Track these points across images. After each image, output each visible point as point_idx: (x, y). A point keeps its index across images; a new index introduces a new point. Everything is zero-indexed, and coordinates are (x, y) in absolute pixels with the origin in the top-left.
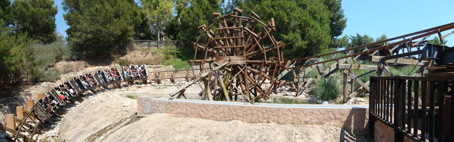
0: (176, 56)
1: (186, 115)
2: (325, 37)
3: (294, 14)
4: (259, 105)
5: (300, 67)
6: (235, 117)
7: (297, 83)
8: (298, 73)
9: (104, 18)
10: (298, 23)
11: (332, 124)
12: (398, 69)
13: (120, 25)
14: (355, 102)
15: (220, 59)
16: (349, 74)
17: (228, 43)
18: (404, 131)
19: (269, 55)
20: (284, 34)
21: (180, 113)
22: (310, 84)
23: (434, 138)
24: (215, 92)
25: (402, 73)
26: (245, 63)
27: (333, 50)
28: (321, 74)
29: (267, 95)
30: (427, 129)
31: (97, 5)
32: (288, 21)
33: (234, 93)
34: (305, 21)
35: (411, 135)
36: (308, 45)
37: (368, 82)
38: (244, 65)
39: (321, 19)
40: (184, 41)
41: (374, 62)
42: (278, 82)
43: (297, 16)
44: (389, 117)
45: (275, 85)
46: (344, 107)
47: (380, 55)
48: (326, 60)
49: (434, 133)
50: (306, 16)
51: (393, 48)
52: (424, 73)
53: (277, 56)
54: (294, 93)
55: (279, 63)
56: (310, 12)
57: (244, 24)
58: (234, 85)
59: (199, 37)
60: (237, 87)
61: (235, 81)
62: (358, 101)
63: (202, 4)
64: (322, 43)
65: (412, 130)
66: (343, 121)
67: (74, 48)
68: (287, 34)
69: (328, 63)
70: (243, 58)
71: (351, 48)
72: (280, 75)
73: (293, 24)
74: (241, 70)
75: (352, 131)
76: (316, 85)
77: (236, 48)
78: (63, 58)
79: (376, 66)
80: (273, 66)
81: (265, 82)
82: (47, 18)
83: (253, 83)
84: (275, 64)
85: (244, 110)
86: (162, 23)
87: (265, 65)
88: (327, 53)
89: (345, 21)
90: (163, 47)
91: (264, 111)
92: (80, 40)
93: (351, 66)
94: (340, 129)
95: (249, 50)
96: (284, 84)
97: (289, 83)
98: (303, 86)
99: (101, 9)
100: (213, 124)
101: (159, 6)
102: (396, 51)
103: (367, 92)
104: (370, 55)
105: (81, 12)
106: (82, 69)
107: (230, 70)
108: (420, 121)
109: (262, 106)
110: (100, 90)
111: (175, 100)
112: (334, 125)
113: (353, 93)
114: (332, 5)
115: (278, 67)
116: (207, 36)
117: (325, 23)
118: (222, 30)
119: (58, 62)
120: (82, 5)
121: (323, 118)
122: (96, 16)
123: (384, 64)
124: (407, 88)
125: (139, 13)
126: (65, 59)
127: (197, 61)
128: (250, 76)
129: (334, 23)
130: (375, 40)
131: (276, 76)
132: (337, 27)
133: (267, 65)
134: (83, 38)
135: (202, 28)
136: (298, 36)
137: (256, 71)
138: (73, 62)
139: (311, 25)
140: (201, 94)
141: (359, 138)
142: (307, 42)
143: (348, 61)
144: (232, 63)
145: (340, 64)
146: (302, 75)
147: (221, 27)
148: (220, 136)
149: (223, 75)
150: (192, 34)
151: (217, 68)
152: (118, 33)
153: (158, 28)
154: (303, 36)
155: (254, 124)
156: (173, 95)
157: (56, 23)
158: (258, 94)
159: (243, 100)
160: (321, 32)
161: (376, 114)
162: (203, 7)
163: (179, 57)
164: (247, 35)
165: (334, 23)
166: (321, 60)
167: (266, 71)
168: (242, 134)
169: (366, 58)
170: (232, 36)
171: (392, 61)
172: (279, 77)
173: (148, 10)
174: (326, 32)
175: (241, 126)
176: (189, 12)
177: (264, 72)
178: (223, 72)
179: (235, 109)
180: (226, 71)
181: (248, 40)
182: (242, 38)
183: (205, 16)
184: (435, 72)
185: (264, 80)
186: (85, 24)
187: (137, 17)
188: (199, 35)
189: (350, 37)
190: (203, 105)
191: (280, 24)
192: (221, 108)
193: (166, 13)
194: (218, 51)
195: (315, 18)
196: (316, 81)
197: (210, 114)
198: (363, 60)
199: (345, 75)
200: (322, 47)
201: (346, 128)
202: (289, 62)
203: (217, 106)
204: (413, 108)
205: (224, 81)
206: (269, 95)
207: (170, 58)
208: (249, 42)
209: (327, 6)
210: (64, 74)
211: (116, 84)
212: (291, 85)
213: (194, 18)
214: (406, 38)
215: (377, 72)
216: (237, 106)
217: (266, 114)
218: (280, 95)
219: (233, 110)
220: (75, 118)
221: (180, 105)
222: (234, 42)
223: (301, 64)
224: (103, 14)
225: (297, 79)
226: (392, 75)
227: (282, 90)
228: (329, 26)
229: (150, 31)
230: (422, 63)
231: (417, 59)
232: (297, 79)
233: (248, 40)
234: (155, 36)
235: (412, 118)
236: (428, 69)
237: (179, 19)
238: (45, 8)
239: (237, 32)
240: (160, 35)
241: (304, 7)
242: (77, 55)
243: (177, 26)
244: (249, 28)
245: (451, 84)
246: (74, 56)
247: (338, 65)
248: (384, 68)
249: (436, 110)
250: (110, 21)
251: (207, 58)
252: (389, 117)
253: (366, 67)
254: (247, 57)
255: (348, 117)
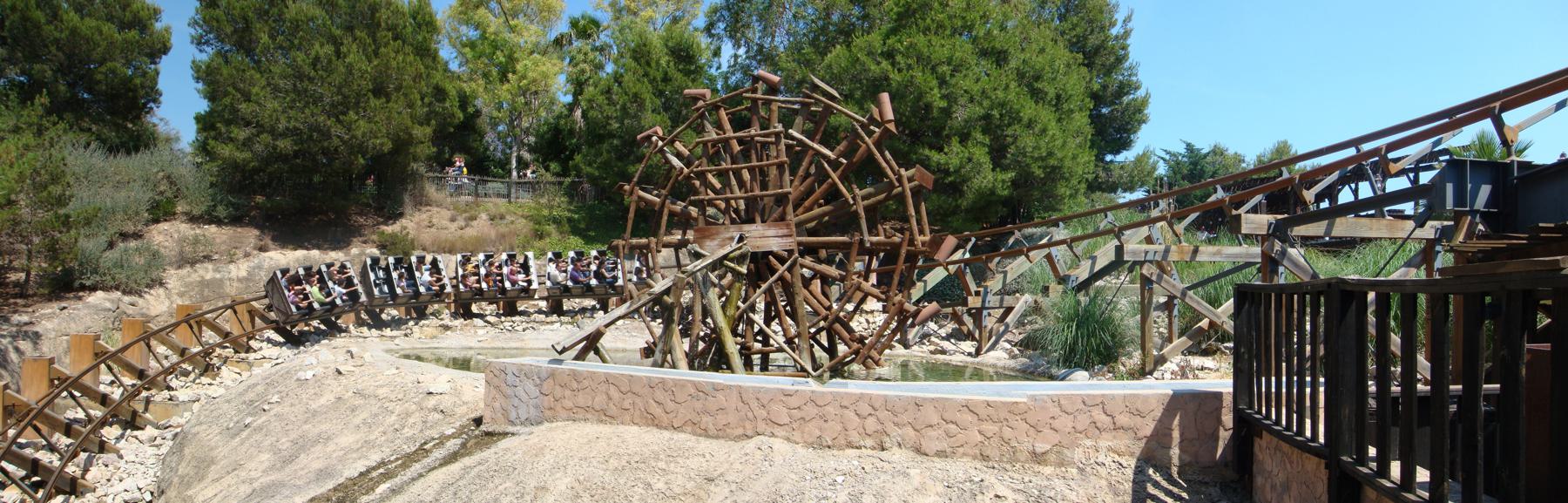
0: (567, 227)
1: (605, 416)
2: (1074, 157)
3: (964, 83)
4: (846, 385)
5: (990, 259)
6: (761, 427)
7: (980, 310)
8: (980, 277)
9: (339, 92)
10: (979, 111)
11: (1104, 443)
12: (1336, 254)
13: (388, 118)
14: (1183, 372)
15: (710, 236)
16: (1160, 278)
17: (734, 182)
18: (1365, 470)
19: (876, 215)
20: (931, 147)
21: (586, 409)
22: (1024, 315)
23: (1484, 497)
24: (693, 346)
25: (1351, 268)
26: (795, 247)
27: (1101, 199)
28: (1062, 280)
29: (874, 353)
30: (1453, 463)
31: (317, 46)
32: (943, 104)
33: (758, 346)
34: (1002, 105)
35: (1389, 485)
36: (1015, 183)
37: (1228, 305)
38: (791, 252)
39: (1058, 97)
40: (593, 180)
41: (1246, 236)
42: (913, 308)
43: (976, 88)
44: (1308, 422)
45: (903, 320)
46: (1145, 387)
47: (1271, 209)
48: (1079, 233)
49: (1480, 479)
50: (1007, 86)
51: (1317, 183)
52: (1438, 264)
53: (906, 219)
54: (968, 346)
55: (911, 242)
56: (1021, 75)
57: (787, 119)
58: (759, 318)
59: (641, 167)
60: (768, 325)
61: (761, 306)
62: (1192, 370)
63: (648, 64)
64: (1063, 177)
65: (1395, 468)
66: (1141, 434)
67: (223, 182)
68: (940, 150)
69: (1086, 242)
70: (785, 231)
71: (1165, 190)
72: (920, 285)
73: (960, 115)
74: (782, 269)
75: (1174, 471)
76: (1044, 317)
77: (762, 197)
78: (179, 209)
79: (1257, 250)
80: (891, 254)
81: (866, 307)
82: (128, 63)
83: (824, 312)
84: (898, 246)
85: (794, 402)
86: (525, 124)
87: (863, 250)
88: (1081, 210)
89: (1145, 102)
90: (526, 200)
91: (865, 409)
92: (247, 155)
93: (1167, 251)
94: (1133, 463)
95: (807, 203)
96: (934, 317)
97: (950, 310)
98: (1002, 319)
99: (330, 61)
100: (692, 449)
101: (514, 72)
102: (1331, 193)
103: (1224, 338)
104: (1234, 212)
105: (258, 62)
106: (247, 255)
107: (744, 270)
108: (1423, 437)
109: (858, 391)
110: (309, 333)
111: (569, 364)
112: (1110, 449)
113: (1176, 342)
114: (1097, 50)
115: (912, 258)
116: (667, 161)
117: (1072, 111)
118: (715, 143)
119: (157, 221)
120: (265, 38)
121: (1070, 425)
122: (311, 80)
123: (1283, 241)
124: (1371, 319)
125: (453, 93)
126: (186, 214)
127: (634, 241)
128: (812, 287)
129: (1104, 111)
130: (1250, 161)
131: (906, 285)
132: (1114, 121)
133: (871, 252)
134: (258, 148)
135: (649, 137)
136: (981, 155)
137: (833, 271)
138: (213, 228)
139: (1025, 120)
140: (648, 352)
141: (1198, 493)
142: (1011, 175)
143: (1156, 233)
144: (748, 247)
145: (1128, 247)
146: (995, 284)
147: (712, 134)
148: (720, 491)
149: (721, 287)
150: (620, 158)
151: (700, 264)
152: (382, 145)
153: (513, 137)
154: (998, 155)
155: (829, 452)
156: (564, 350)
157: (162, 84)
158: (842, 349)
159: (790, 371)
160: (1059, 142)
161: (1260, 412)
162: (652, 72)
163: (576, 231)
164: (797, 154)
165: (1104, 111)
166: (1061, 233)
167: (868, 270)
168: (787, 487)
169: (1218, 222)
170: (747, 158)
171: (1315, 229)
172: (917, 292)
173: (481, 82)
174: (1078, 140)
175: (784, 456)
176: (608, 91)
177: (859, 274)
178: (721, 277)
179: (763, 399)
180: (729, 275)
181: (801, 172)
182: (780, 166)
183: (658, 102)
184: (1480, 260)
185: (863, 301)
186: (272, 104)
187: (447, 104)
188: (640, 159)
189: (1163, 155)
190: (663, 382)
191: (914, 113)
192: (720, 396)
193: (536, 93)
194: (703, 211)
195: (1037, 95)
196: (1045, 302)
197: (684, 413)
198: (1210, 229)
199: (1146, 282)
200: (1062, 190)
201: (1152, 457)
202: (951, 241)
203: (708, 389)
204: (1395, 389)
205: (724, 307)
206: (880, 353)
207: (549, 235)
208: (805, 178)
209: (1080, 56)
210: (179, 267)
211: (367, 312)
212: (956, 318)
213: (624, 108)
214: (1366, 147)
215: (1259, 270)
216: (768, 390)
217: (871, 420)
218: (920, 352)
219: (754, 404)
220: (231, 433)
221: (586, 383)
222: (753, 179)
223: (991, 248)
224: (337, 79)
225: (980, 299)
226: (1315, 276)
227: (926, 336)
228: (1086, 120)
229: (487, 149)
230: (1429, 230)
231: (1408, 217)
232: (980, 299)
233: (801, 172)
234: (504, 164)
235: (1395, 424)
236: (1452, 250)
237: (578, 113)
238: (123, 26)
239: (765, 145)
240: (520, 159)
241: (1000, 57)
242: (233, 205)
243: (571, 132)
244: (802, 133)
245: (1549, 302)
246: (220, 208)
247: (1119, 250)
248: (1284, 253)
249: (1488, 397)
250: (357, 104)
251: (668, 233)
252: (1308, 422)
253: (1218, 253)
254: (798, 225)
255: (1160, 421)
